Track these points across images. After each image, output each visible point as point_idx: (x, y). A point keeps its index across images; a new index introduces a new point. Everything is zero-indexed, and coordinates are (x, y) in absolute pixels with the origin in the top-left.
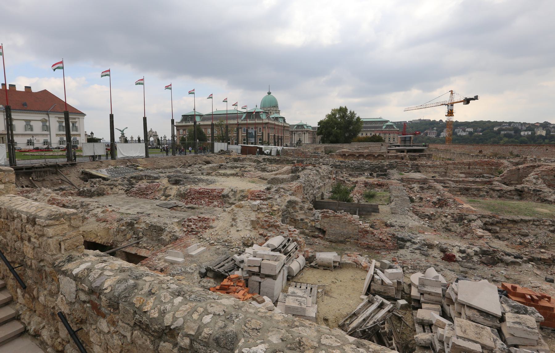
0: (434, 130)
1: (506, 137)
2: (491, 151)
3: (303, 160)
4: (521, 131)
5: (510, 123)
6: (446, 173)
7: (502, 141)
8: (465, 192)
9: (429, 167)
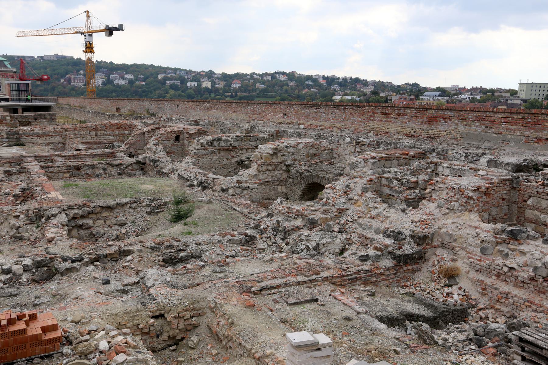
0: (80, 74)
1: (173, 89)
2: (129, 108)
4: (187, 81)
5: (176, 70)
6: (64, 144)
7: (168, 95)
8: (76, 172)
9: (38, 135)
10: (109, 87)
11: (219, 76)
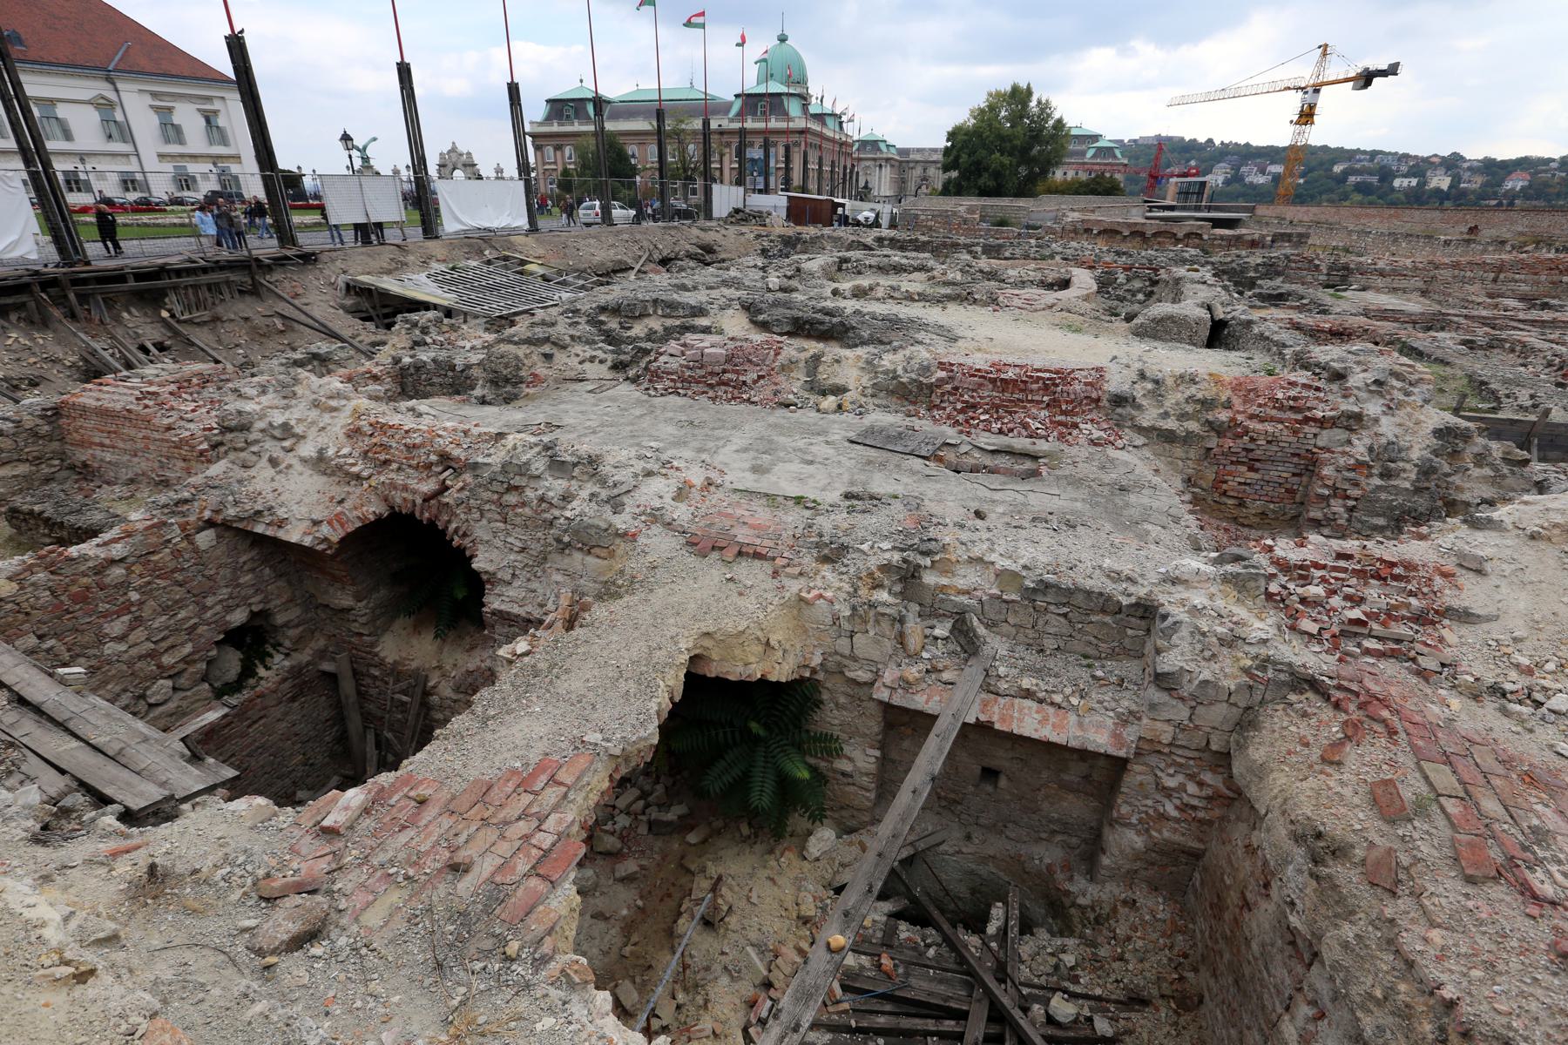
3: (1000, 246)
4: (1396, 177)
5: (1374, 154)
9: (1382, 274)
10: (1236, 187)
11: (1475, 164)
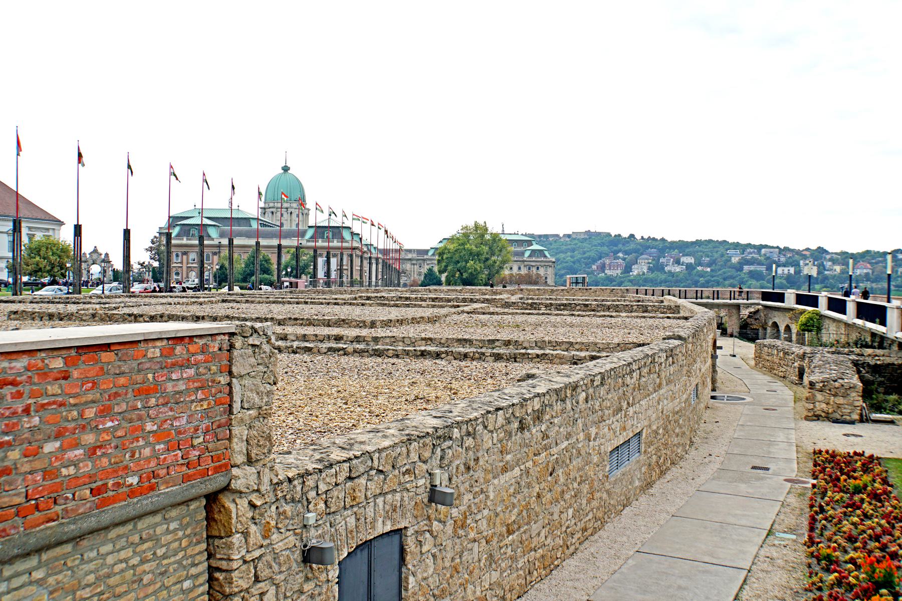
0: (618, 258)
